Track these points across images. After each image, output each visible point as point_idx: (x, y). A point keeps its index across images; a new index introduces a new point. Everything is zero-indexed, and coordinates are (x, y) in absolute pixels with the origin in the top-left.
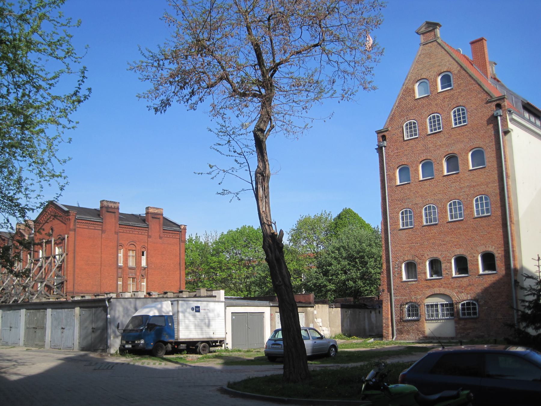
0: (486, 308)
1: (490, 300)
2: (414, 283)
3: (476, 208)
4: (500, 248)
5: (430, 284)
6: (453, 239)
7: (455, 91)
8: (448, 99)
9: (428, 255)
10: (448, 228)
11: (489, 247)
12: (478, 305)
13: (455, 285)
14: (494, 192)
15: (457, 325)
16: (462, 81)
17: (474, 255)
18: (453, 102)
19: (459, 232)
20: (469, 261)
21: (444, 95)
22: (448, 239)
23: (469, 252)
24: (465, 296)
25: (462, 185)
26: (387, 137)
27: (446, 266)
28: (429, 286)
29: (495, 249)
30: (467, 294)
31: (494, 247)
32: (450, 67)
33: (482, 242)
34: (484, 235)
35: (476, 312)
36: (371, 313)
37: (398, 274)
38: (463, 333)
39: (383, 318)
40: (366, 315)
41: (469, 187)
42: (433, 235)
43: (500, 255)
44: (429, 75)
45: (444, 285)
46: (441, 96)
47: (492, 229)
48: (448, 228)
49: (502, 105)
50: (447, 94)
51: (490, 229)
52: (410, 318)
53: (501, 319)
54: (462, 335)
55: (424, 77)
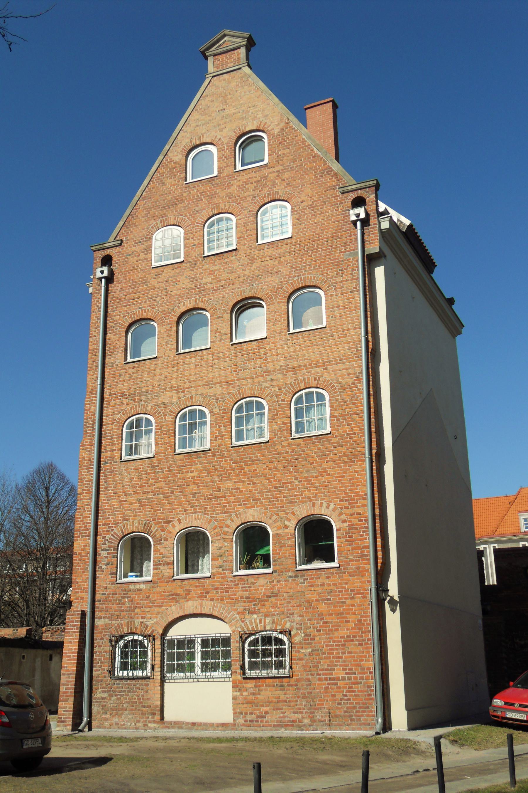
0: (309, 650)
1: (319, 631)
2: (142, 586)
3: (296, 418)
4: (346, 508)
5: (179, 591)
6: (240, 486)
7: (271, 170)
8: (255, 184)
9: (179, 520)
10: (231, 460)
11: (321, 506)
12: (290, 642)
13: (239, 594)
14: (340, 383)
15: (238, 694)
16: (287, 151)
17: (287, 523)
18: (265, 191)
19: (255, 470)
20: (184, 612)
21: (246, 177)
22: (229, 484)
23: (275, 517)
24: (261, 622)
25: (270, 366)
26: (114, 259)
27: (220, 548)
28: (177, 595)
29: (334, 510)
30: (267, 615)
31: (332, 506)
32: (265, 121)
33: (306, 494)
34: (313, 477)
35: (250, 657)
36: (51, 659)
37: (107, 564)
38: (251, 713)
39: (63, 671)
40: (250, 627)
41: (286, 370)
42: (195, 474)
43: (346, 525)
44: (218, 137)
45: (212, 593)
46: (242, 178)
47: (330, 464)
48: (231, 460)
49: (367, 199)
50: (253, 175)
51: (325, 465)
52: (126, 672)
53: (344, 679)
54: (249, 718)
55: (208, 140)
